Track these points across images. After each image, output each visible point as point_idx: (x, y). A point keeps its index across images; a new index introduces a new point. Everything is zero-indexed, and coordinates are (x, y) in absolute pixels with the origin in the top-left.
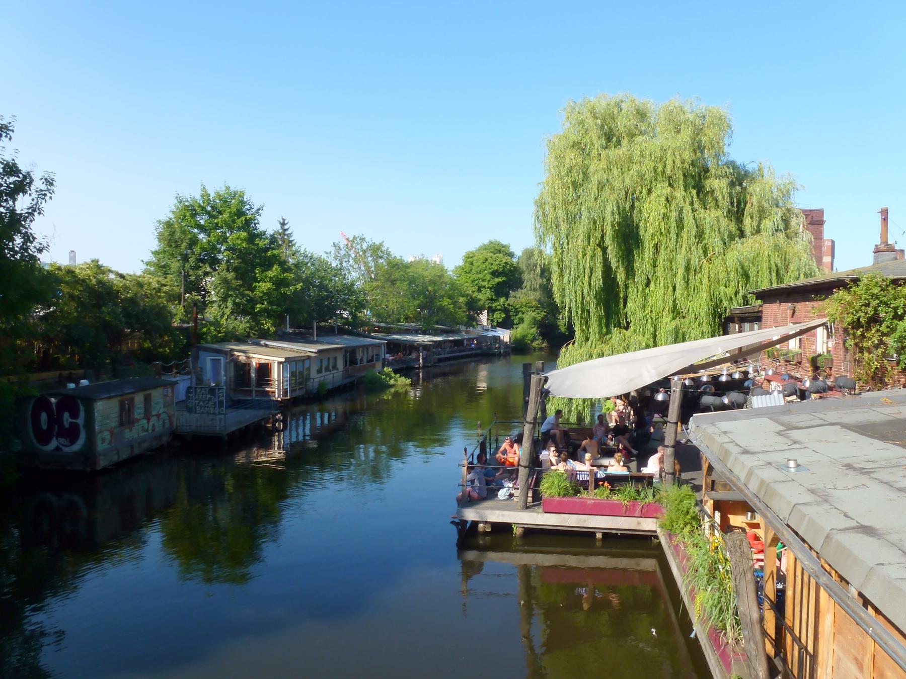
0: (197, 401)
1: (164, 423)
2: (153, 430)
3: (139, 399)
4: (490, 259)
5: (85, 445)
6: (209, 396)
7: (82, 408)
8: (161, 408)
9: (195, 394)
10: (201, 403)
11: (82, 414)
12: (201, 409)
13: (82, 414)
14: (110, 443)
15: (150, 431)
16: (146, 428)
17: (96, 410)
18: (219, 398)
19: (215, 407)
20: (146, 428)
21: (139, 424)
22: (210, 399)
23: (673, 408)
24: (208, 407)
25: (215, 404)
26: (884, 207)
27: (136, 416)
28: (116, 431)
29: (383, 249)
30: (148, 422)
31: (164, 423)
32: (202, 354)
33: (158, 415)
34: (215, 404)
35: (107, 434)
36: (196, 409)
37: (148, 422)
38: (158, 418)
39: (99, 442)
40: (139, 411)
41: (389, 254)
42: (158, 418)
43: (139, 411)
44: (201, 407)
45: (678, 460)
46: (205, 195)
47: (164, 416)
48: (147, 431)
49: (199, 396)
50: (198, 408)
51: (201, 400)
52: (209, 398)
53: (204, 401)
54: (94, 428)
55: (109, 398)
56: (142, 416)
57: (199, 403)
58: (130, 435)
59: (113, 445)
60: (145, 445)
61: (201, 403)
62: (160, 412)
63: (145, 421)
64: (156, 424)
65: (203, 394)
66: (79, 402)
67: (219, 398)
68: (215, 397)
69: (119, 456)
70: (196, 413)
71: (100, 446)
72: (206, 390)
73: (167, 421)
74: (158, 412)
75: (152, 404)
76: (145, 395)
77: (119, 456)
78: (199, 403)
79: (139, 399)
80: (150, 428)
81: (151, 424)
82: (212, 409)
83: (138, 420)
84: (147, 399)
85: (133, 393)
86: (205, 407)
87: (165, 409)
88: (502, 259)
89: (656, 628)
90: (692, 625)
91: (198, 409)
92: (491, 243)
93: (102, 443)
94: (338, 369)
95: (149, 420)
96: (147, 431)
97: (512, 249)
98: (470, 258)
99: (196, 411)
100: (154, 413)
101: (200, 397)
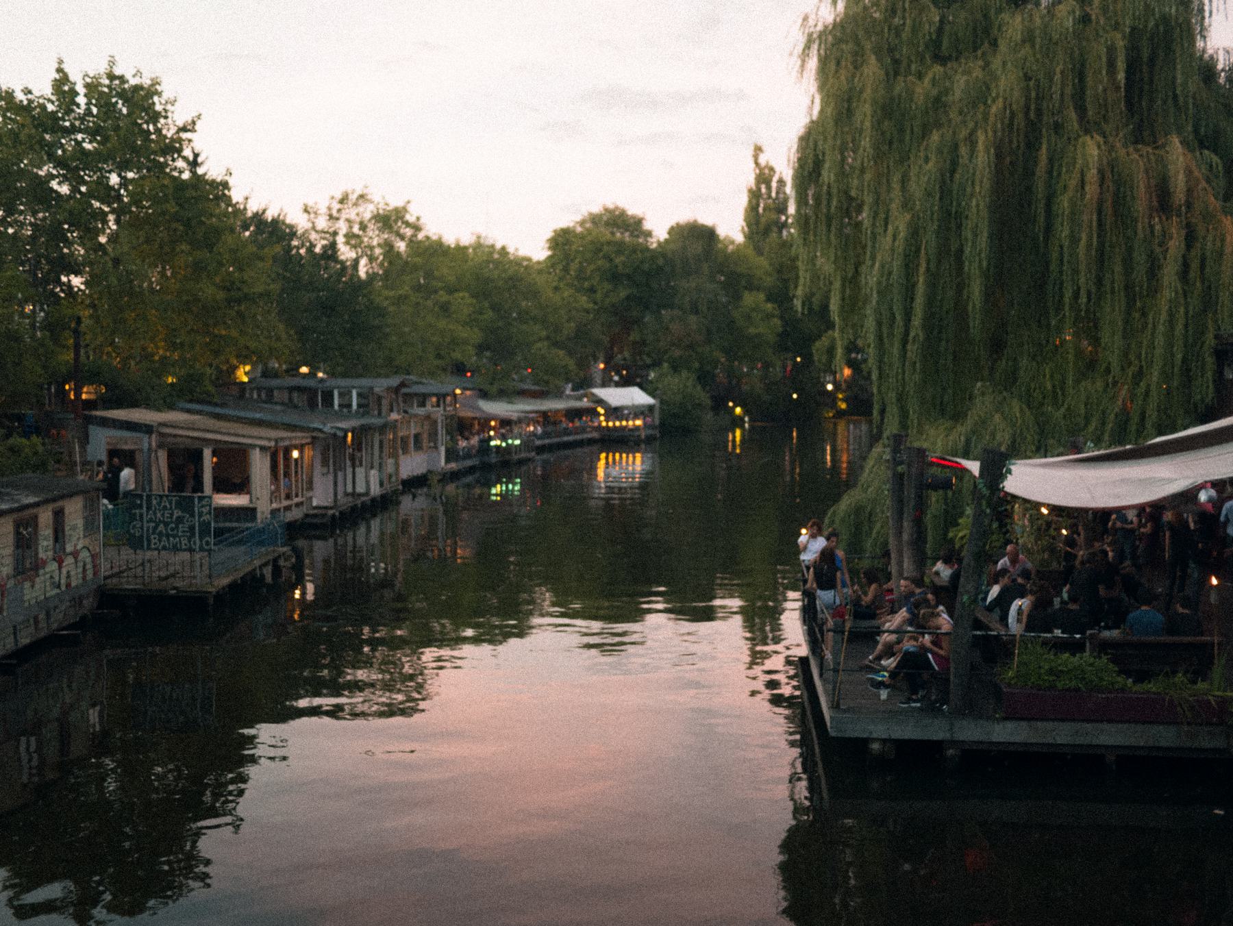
1: (84, 570)
2: (68, 585)
3: (45, 517)
6: (177, 513)
8: (79, 539)
9: (149, 508)
10: (161, 527)
12: (160, 541)
15: (63, 588)
18: (200, 515)
21: (47, 570)
22: (180, 520)
24: (174, 536)
25: (192, 528)
26: (764, 148)
27: (42, 555)
29: (408, 217)
30: (60, 567)
31: (84, 570)
34: (192, 528)
36: (149, 541)
37: (60, 567)
40: (45, 543)
41: (417, 228)
42: (76, 558)
43: (45, 543)
45: (172, 597)
47: (85, 555)
49: (155, 513)
52: (178, 517)
57: (155, 528)
58: (36, 591)
60: (58, 617)
61: (161, 527)
63: (55, 566)
64: (72, 573)
67: (200, 515)
68: (192, 515)
69: (16, 641)
70: (149, 548)
75: (67, 528)
77: (16, 641)
78: (155, 528)
79: (45, 517)
80: (63, 581)
81: (64, 571)
84: (59, 515)
87: (87, 541)
89: (1223, 816)
90: (784, 868)
95: (60, 563)
96: (59, 586)
98: (562, 241)
99: (149, 544)
100: (69, 548)
101: (159, 515)
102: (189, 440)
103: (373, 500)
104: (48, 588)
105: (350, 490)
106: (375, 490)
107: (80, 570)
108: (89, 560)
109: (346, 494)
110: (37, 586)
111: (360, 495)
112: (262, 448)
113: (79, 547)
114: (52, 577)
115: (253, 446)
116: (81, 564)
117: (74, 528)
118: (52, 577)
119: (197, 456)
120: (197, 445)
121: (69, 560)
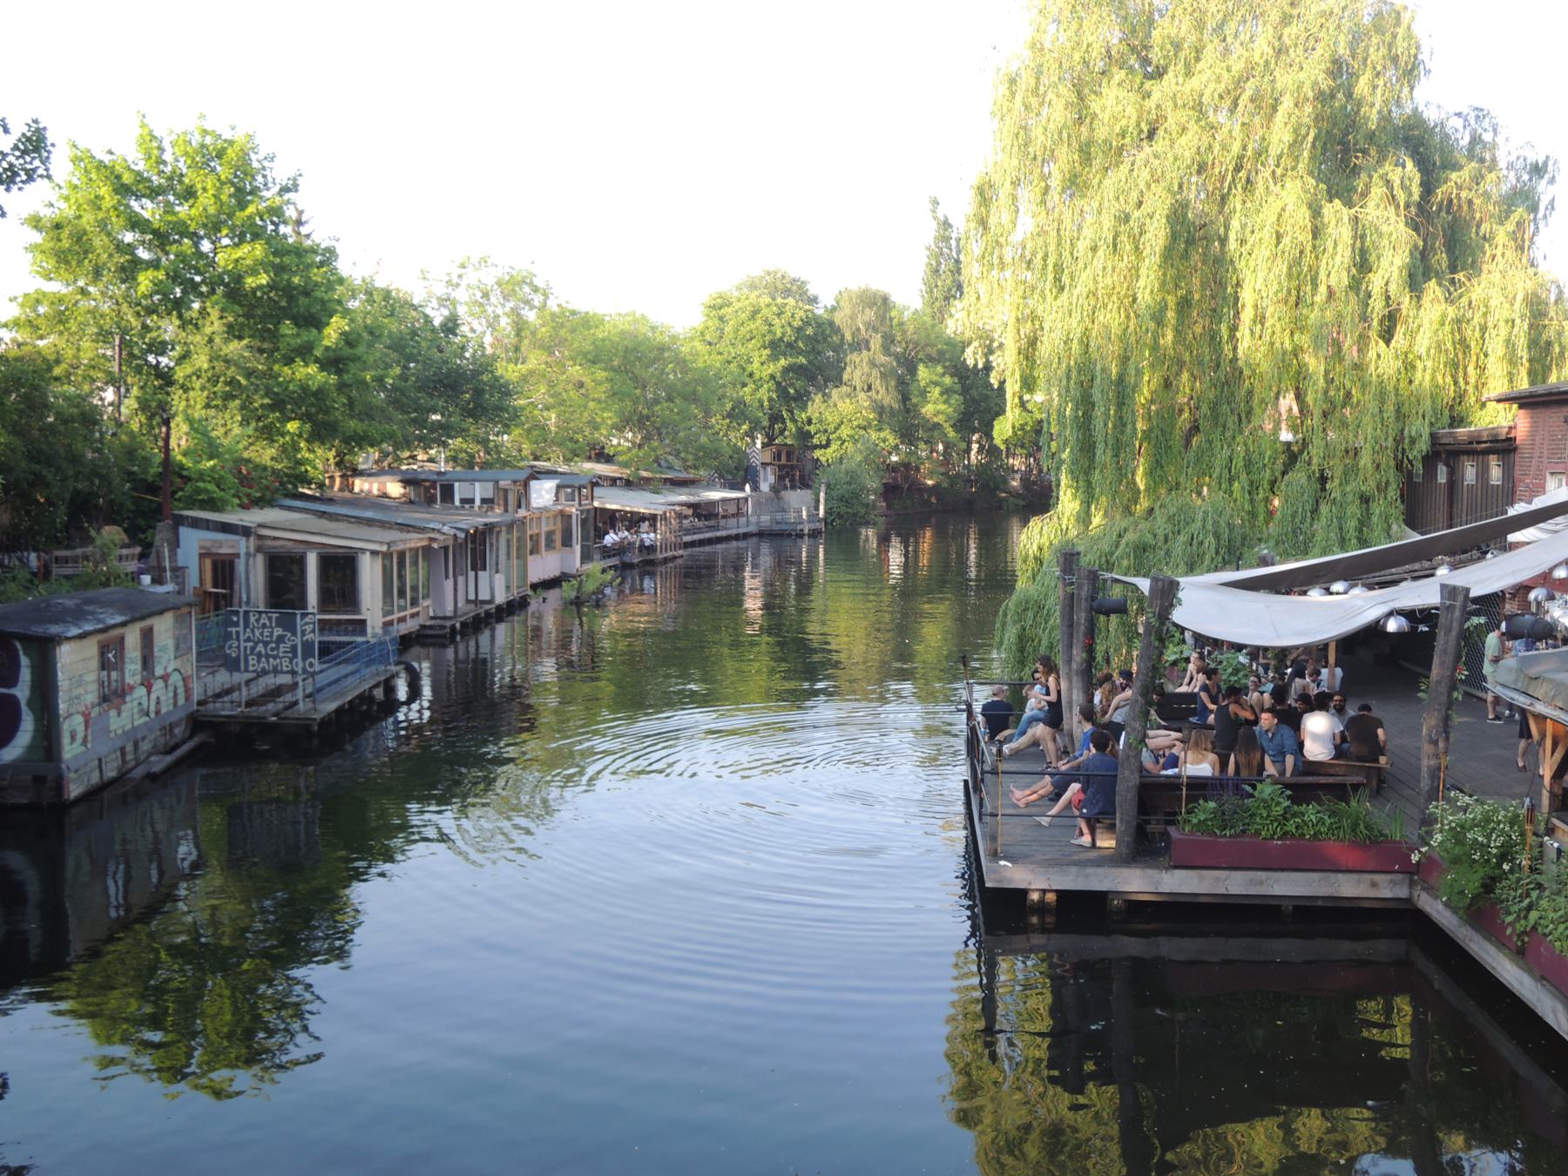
0: (250, 644)
1: (176, 695)
2: (157, 712)
3: (132, 637)
4: (765, 311)
5: (31, 748)
6: (278, 632)
7: (24, 661)
9: (246, 625)
11: (25, 674)
13: (25, 674)
14: (85, 741)
15: (152, 715)
16: (145, 706)
17: (59, 665)
19: (295, 656)
20: (145, 706)
22: (281, 639)
23: (1446, 642)
24: (275, 657)
28: (95, 712)
31: (176, 695)
32: (184, 532)
33: (165, 678)
34: (294, 648)
35: (79, 720)
38: (166, 682)
39: (66, 740)
40: (133, 667)
42: (166, 682)
43: (133, 667)
44: (259, 655)
46: (151, 144)
47: (175, 679)
48: (147, 714)
50: (252, 660)
51: (259, 641)
53: (266, 644)
54: (57, 704)
55: (82, 637)
56: (138, 678)
57: (253, 649)
59: (89, 745)
61: (260, 648)
62: (170, 670)
63: (143, 691)
64: (163, 699)
65: (264, 626)
66: (18, 646)
68: (294, 634)
71: (70, 751)
72: (270, 619)
73: (181, 691)
74: (165, 668)
75: (156, 649)
76: (141, 630)
78: (253, 649)
79: (132, 637)
80: (152, 708)
81: (153, 697)
82: (286, 662)
83: (132, 688)
84: (148, 635)
85: (124, 624)
86: (267, 656)
88: (795, 310)
91: (251, 662)
92: (865, 291)
93: (72, 743)
94: (1443, 587)
95: (149, 688)
96: (147, 714)
97: (812, 290)
98: (718, 307)
100: (159, 671)
101: (257, 633)
102: (291, 543)
103: (499, 608)
104: (136, 717)
105: (472, 597)
106: (501, 598)
107: (171, 694)
108: (180, 684)
109: (468, 601)
110: (124, 714)
111: (484, 602)
112: (374, 553)
113: (170, 670)
114: (140, 704)
115: (363, 550)
116: (171, 689)
117: (164, 649)
118: (140, 704)
119: (301, 561)
120: (300, 549)
121: (158, 685)
